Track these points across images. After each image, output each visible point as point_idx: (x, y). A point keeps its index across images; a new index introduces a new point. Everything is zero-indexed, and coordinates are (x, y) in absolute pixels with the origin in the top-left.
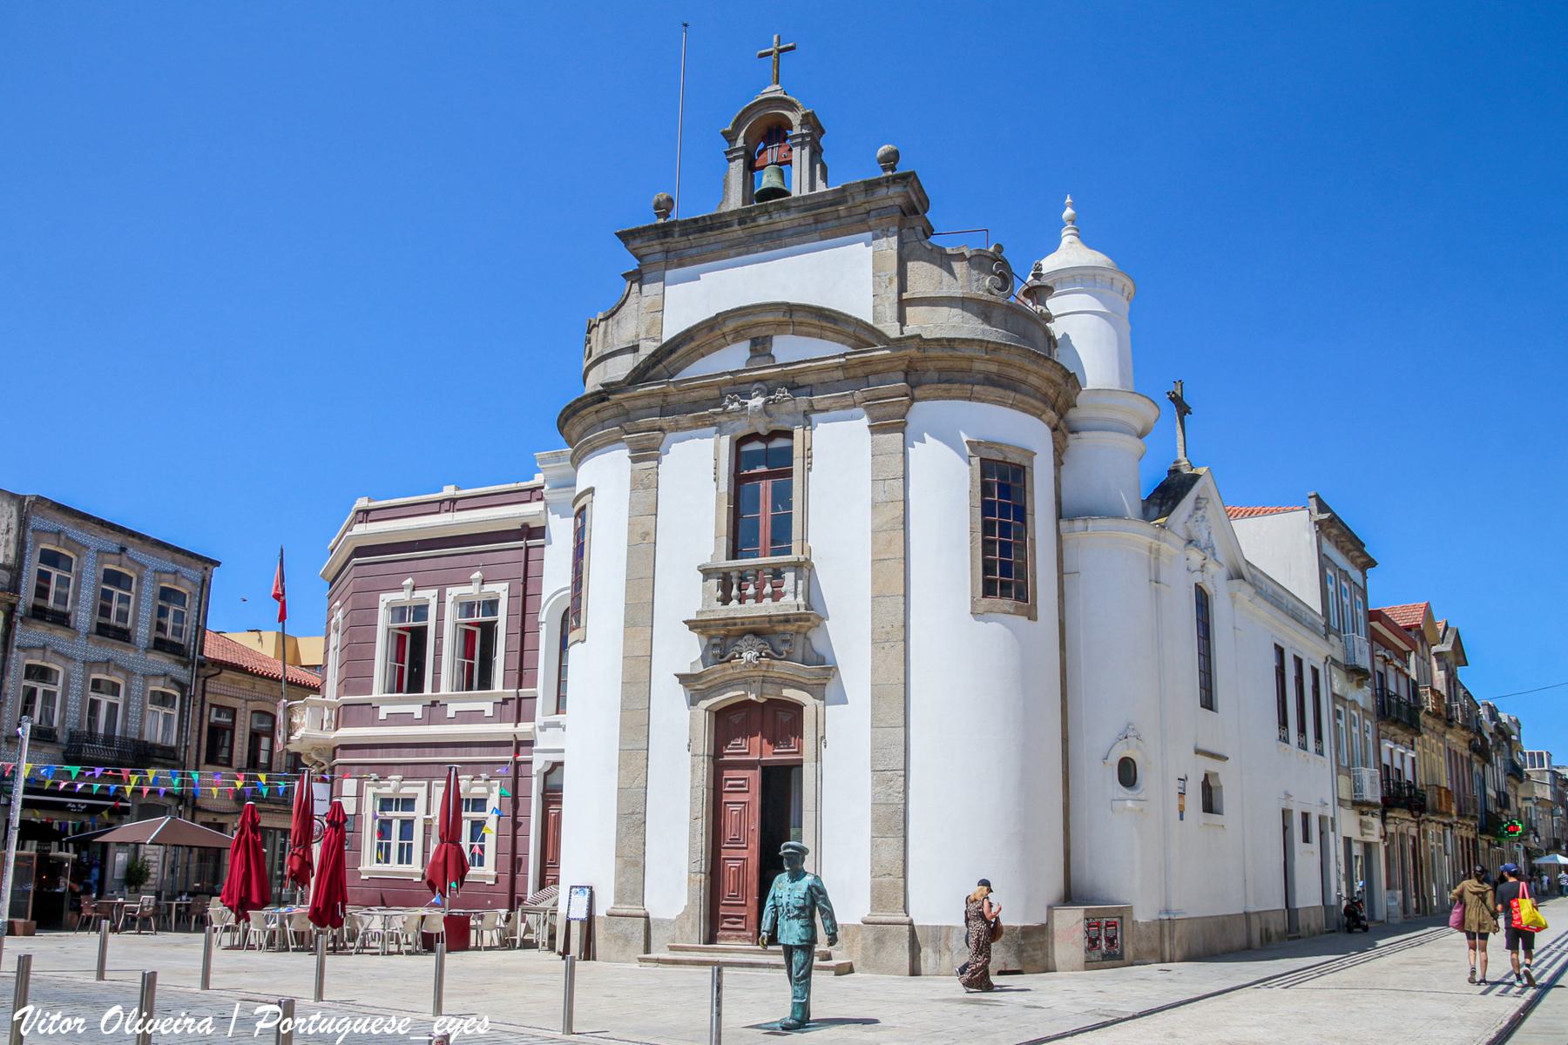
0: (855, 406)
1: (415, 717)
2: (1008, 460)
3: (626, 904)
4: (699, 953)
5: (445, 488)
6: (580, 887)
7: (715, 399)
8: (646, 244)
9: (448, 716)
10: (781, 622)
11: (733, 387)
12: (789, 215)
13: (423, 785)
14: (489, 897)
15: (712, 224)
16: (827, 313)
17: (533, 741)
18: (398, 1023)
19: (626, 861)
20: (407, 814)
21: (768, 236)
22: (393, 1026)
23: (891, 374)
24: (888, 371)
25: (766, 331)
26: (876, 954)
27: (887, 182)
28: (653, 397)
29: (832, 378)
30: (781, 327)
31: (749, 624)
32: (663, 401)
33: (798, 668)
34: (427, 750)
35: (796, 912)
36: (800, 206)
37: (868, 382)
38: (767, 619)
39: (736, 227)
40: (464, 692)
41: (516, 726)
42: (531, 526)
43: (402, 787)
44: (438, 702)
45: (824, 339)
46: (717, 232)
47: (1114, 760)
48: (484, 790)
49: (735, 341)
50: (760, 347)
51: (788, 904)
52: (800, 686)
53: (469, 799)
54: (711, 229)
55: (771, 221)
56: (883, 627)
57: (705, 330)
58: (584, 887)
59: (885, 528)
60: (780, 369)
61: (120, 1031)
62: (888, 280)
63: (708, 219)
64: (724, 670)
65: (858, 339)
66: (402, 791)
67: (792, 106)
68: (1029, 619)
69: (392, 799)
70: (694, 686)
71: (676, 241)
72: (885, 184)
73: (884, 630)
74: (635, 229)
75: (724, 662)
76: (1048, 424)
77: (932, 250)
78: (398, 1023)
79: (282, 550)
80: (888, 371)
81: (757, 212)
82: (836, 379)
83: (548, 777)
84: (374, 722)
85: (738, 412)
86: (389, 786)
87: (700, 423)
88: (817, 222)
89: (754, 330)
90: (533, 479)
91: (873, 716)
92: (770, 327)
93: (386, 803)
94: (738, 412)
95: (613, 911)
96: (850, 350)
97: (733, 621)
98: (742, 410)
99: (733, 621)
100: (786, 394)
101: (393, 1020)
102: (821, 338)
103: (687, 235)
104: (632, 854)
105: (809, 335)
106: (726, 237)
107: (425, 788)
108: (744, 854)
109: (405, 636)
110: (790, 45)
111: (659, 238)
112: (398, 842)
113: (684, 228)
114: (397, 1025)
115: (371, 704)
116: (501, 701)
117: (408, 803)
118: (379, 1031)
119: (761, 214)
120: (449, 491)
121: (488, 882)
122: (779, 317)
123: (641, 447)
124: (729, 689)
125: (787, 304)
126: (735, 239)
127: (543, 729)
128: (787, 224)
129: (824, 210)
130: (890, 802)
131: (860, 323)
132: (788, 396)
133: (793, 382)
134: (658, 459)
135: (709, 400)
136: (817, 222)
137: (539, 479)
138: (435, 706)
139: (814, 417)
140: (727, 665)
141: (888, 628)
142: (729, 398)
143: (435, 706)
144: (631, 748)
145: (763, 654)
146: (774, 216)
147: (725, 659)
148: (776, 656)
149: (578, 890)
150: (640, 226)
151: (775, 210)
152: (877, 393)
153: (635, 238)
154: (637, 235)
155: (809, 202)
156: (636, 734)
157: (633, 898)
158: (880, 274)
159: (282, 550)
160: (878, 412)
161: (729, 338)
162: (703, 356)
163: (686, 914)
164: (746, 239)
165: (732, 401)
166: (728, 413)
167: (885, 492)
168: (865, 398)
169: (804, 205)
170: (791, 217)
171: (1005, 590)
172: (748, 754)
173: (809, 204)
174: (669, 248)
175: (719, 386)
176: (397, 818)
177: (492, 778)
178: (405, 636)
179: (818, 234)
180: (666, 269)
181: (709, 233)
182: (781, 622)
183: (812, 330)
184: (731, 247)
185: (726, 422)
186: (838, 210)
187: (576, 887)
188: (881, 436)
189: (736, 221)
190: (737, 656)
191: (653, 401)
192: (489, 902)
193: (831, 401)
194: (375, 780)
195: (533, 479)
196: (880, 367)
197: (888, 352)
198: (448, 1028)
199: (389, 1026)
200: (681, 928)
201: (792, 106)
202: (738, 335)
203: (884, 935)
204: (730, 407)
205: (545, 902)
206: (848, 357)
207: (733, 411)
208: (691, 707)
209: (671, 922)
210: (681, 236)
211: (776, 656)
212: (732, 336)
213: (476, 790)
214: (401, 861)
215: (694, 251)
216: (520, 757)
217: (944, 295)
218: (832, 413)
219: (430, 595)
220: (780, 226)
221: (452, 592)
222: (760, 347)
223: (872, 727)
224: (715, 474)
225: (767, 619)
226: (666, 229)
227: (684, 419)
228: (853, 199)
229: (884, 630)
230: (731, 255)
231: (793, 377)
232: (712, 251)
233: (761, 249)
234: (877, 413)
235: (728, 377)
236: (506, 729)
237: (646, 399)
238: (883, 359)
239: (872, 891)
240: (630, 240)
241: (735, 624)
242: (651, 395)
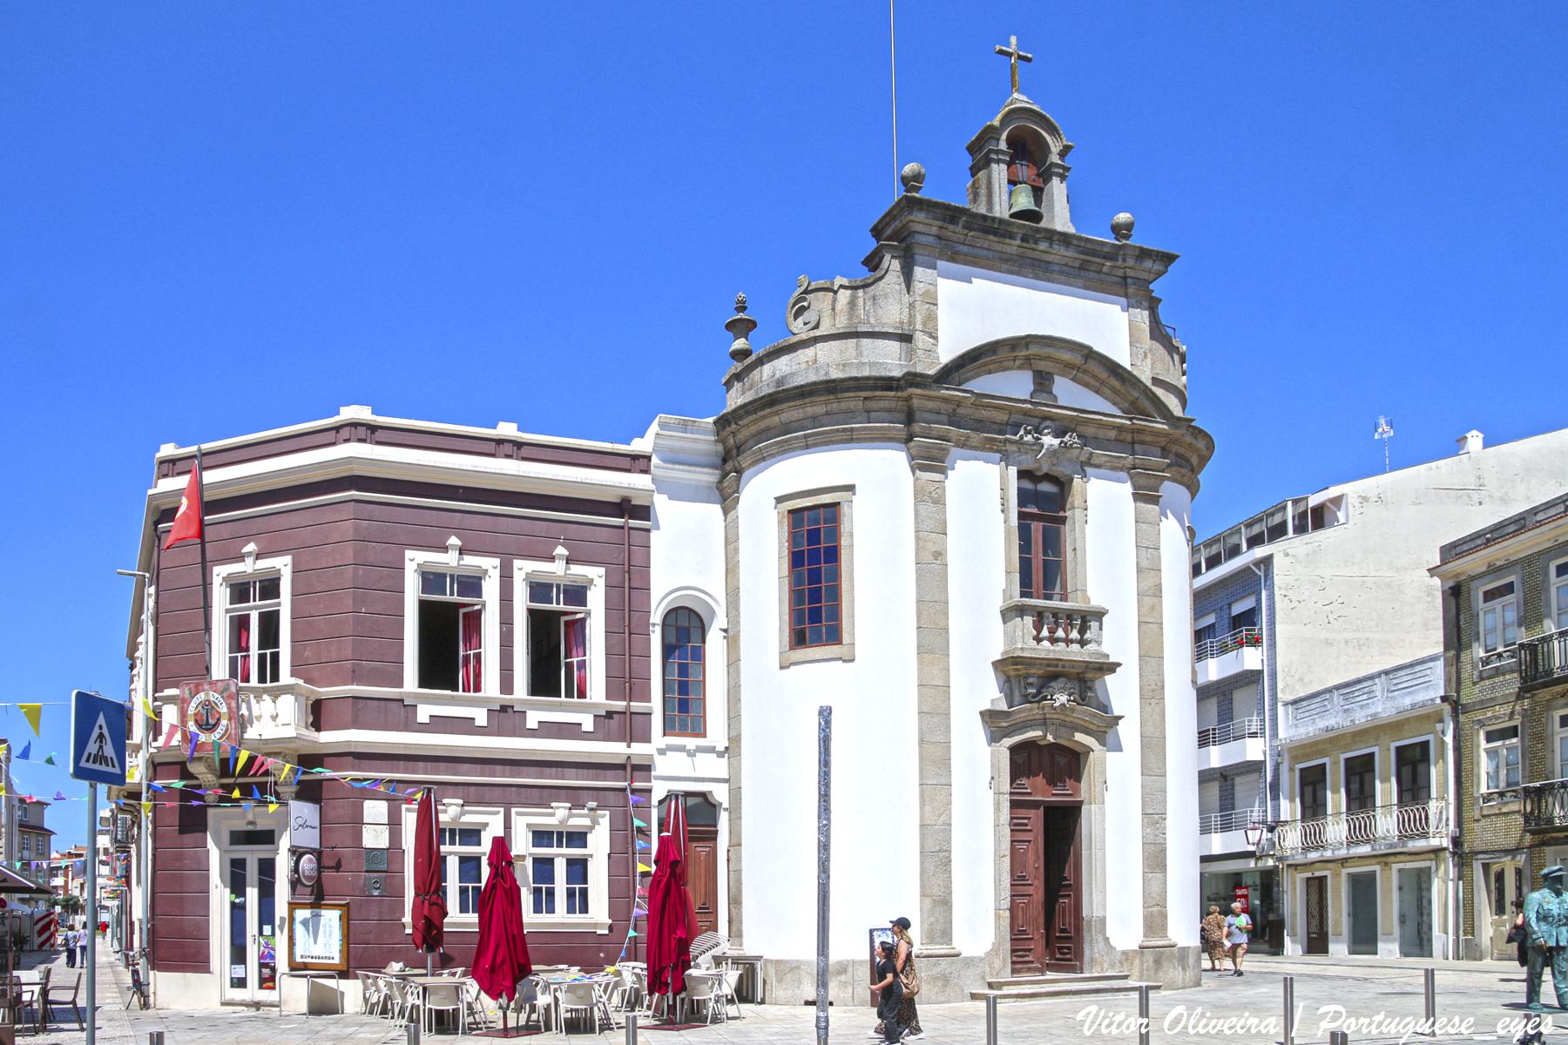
0: (1121, 469)
1: (476, 724)
3: (936, 944)
4: (1030, 986)
5: (342, 409)
6: (882, 929)
7: (1001, 424)
8: (927, 221)
9: (528, 727)
10: (1095, 669)
11: (1022, 417)
13: (498, 813)
14: (600, 950)
15: (998, 229)
16: (1120, 371)
17: (650, 766)
18: (1461, 1021)
19: (934, 900)
21: (1037, 263)
22: (1456, 1027)
23: (1152, 447)
24: (1151, 444)
25: (1052, 367)
26: (1155, 974)
27: (1157, 256)
28: (946, 403)
29: (1106, 436)
30: (1068, 369)
31: (1069, 668)
32: (954, 410)
33: (1094, 715)
34: (442, 765)
35: (1564, 921)
36: (1080, 247)
37: (869, 418)
38: (1084, 664)
39: (1018, 242)
40: (472, 694)
41: (629, 746)
42: (634, 502)
43: (463, 813)
44: (513, 707)
45: (1099, 394)
46: (996, 239)
48: (586, 822)
50: (1043, 382)
51: (1559, 915)
52: (1088, 732)
53: (562, 833)
54: (995, 234)
55: (1049, 249)
57: (1008, 347)
58: (886, 929)
60: (1075, 414)
63: (997, 221)
64: (1031, 710)
65: (1134, 403)
66: (465, 819)
67: (1053, 130)
69: (553, 832)
70: (1000, 723)
71: (957, 231)
72: (1154, 258)
73: (1150, 688)
74: (926, 200)
78: (1461, 1021)
80: (1151, 444)
81: (1042, 236)
82: (1108, 438)
84: (410, 725)
85: (1031, 445)
86: (553, 815)
87: (987, 446)
88: (1081, 268)
89: (1043, 363)
90: (494, 427)
92: (1057, 365)
93: (541, 837)
94: (1031, 445)
95: (1145, 944)
96: (1119, 413)
97: (1056, 662)
98: (1034, 444)
99: (1056, 662)
100: (1076, 440)
101: (1457, 1020)
102: (1097, 392)
103: (971, 229)
104: (940, 893)
105: (1087, 385)
106: (999, 247)
107: (501, 816)
108: (1031, 890)
109: (566, 622)
110: (1030, 56)
111: (944, 220)
112: (458, 885)
113: (970, 220)
114: (1460, 1026)
115: (402, 701)
116: (499, 708)
118: (1536, 1031)
119: (1046, 238)
120: (507, 430)
121: (599, 932)
122: (1076, 359)
123: (928, 455)
124: (1028, 729)
125: (1089, 349)
126: (1005, 253)
127: (662, 752)
128: (1056, 259)
129: (1093, 259)
130: (1158, 842)
131: (1148, 392)
132: (1079, 444)
134: (943, 471)
135: (995, 423)
136: (1081, 268)
137: (640, 445)
138: (506, 712)
139: (1089, 470)
140: (1036, 705)
142: (1025, 429)
143: (506, 712)
144: (935, 783)
146: (1055, 246)
147: (1036, 699)
149: (880, 933)
150: (934, 199)
151: (1057, 240)
152: (1146, 463)
153: (921, 210)
154: (925, 207)
155: (1089, 246)
156: (939, 768)
157: (943, 938)
158: (1137, 345)
160: (1143, 482)
161: (1017, 363)
162: (990, 373)
163: (995, 950)
164: (1016, 258)
165: (1028, 432)
166: (1023, 444)
169: (1083, 247)
170: (1067, 254)
172: (1030, 794)
173: (1089, 249)
174: (1053, 259)
175: (1010, 411)
176: (562, 855)
177: (600, 807)
178: (566, 622)
179: (1083, 281)
181: (991, 237)
182: (1095, 669)
183: (1092, 381)
184: (1007, 261)
185: (1014, 452)
186: (1103, 265)
187: (877, 930)
188: (1144, 505)
189: (1021, 235)
191: (944, 406)
192: (602, 955)
193: (1107, 459)
194: (591, 809)
195: (494, 427)
196: (1148, 439)
197: (1166, 427)
198: (1511, 1028)
199: (1453, 1026)
200: (990, 965)
201: (1053, 130)
202: (1028, 363)
203: (1161, 957)
204: (1025, 439)
205: (715, 949)
206: (1134, 421)
207: (1026, 443)
208: (993, 744)
209: (981, 959)
210: (964, 227)
212: (1021, 362)
213: (574, 822)
214: (571, 910)
215: (965, 249)
216: (635, 784)
217: (825, 333)
218: (1102, 471)
219: (490, 564)
220: (1050, 258)
221: (523, 569)
222: (1043, 382)
223: (1142, 774)
224: (1003, 505)
225: (1084, 664)
226: (956, 214)
227: (976, 437)
228: (1124, 260)
230: (1002, 269)
231: (1077, 425)
232: (988, 258)
233: (1031, 275)
234: (1143, 482)
235: (1029, 406)
236: (615, 749)
237: (939, 403)
238: (1157, 433)
239: (1144, 921)
240: (915, 209)
241: (1057, 666)
242: (945, 400)
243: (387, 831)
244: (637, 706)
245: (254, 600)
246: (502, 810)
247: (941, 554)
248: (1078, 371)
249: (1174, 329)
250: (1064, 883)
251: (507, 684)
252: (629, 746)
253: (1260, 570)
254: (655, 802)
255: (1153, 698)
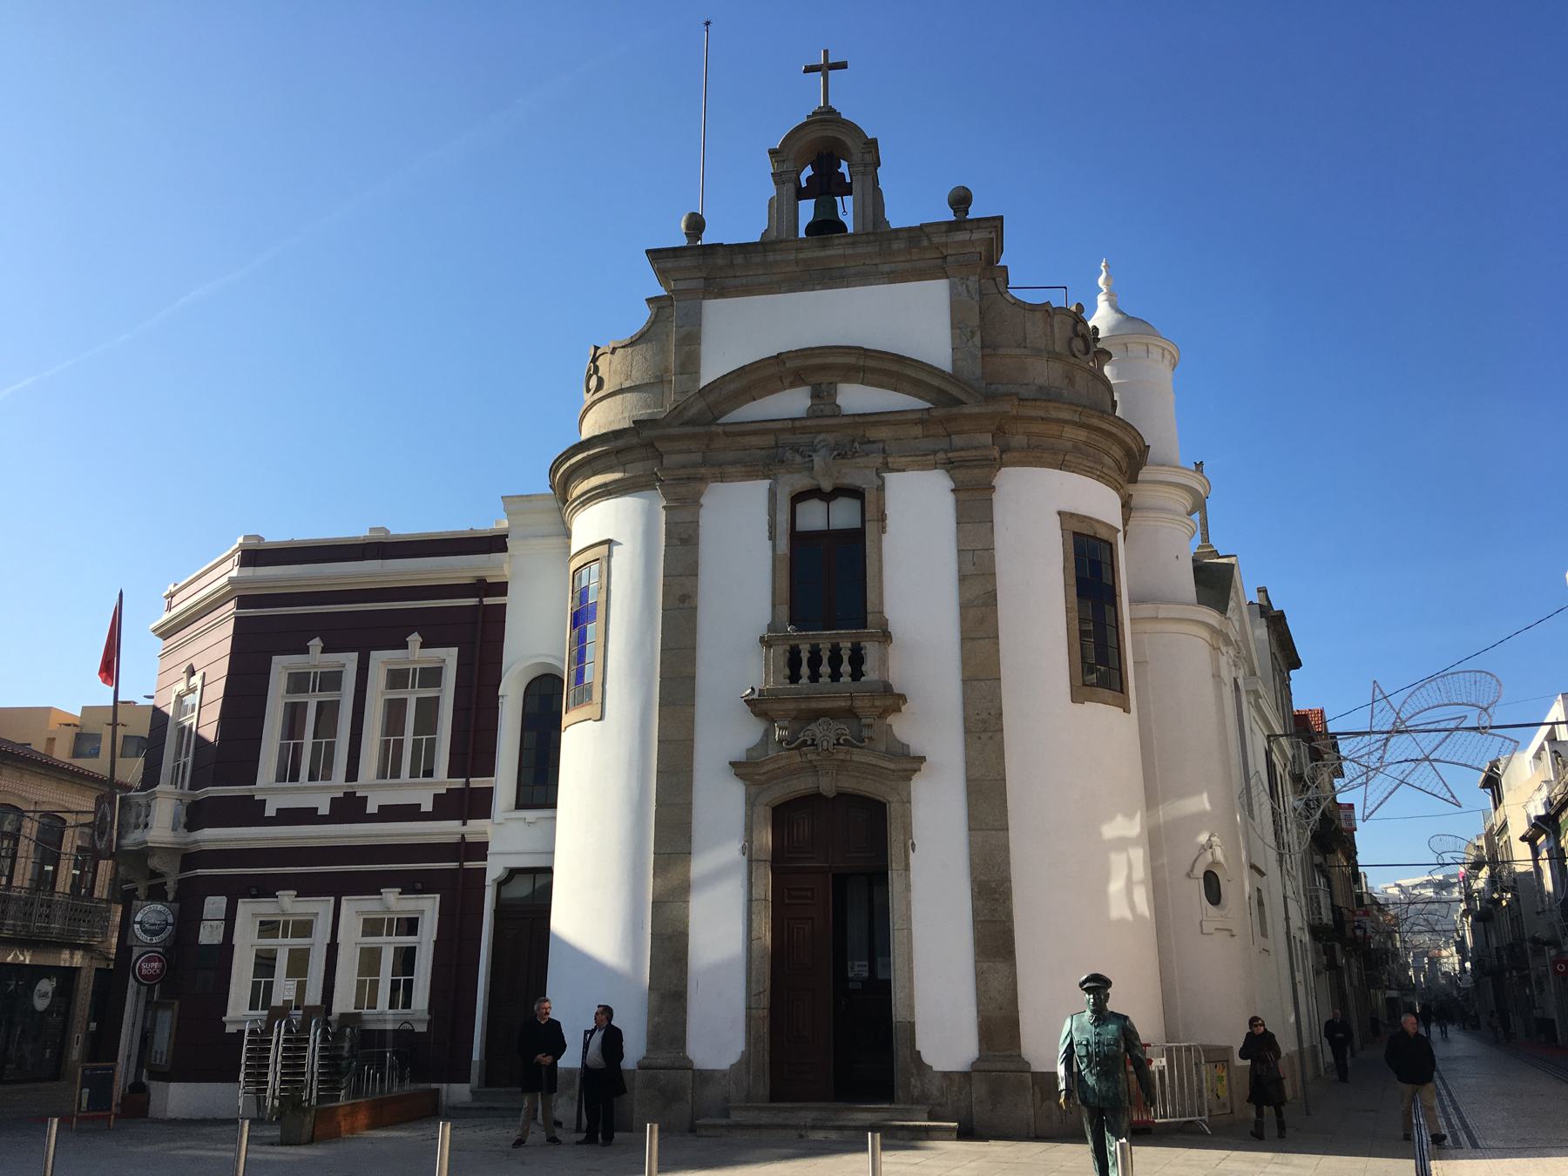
2: (1098, 536)
12: (824, 247)
20: (300, 942)
23: (977, 435)
41: (464, 824)
47: (1199, 872)
49: (792, 385)
50: (822, 395)
56: (978, 714)
59: (975, 603)
61: (663, 1058)
62: (969, 334)
68: (1124, 711)
73: (978, 717)
75: (792, 749)
76: (1122, 498)
77: (1014, 304)
79: (121, 595)
83: (503, 888)
91: (971, 816)
93: (268, 928)
117: (304, 928)
133: (864, 436)
141: (984, 715)
145: (841, 741)
148: (858, 744)
159: (121, 595)
167: (974, 564)
168: (949, 459)
171: (1104, 683)
180: (704, 298)
190: (809, 742)
202: (797, 379)
209: (723, 1073)
211: (858, 744)
219: (350, 660)
221: (382, 661)
222: (822, 395)
229: (978, 717)
236: (447, 830)
243: (223, 926)
244: (477, 782)
245: (415, 670)
246: (332, 899)
247: (689, 597)
248: (864, 372)
249: (1065, 288)
250: (1549, 885)
251: (352, 774)
252: (464, 824)
253: (192, 723)
254: (489, 881)
255: (985, 731)
